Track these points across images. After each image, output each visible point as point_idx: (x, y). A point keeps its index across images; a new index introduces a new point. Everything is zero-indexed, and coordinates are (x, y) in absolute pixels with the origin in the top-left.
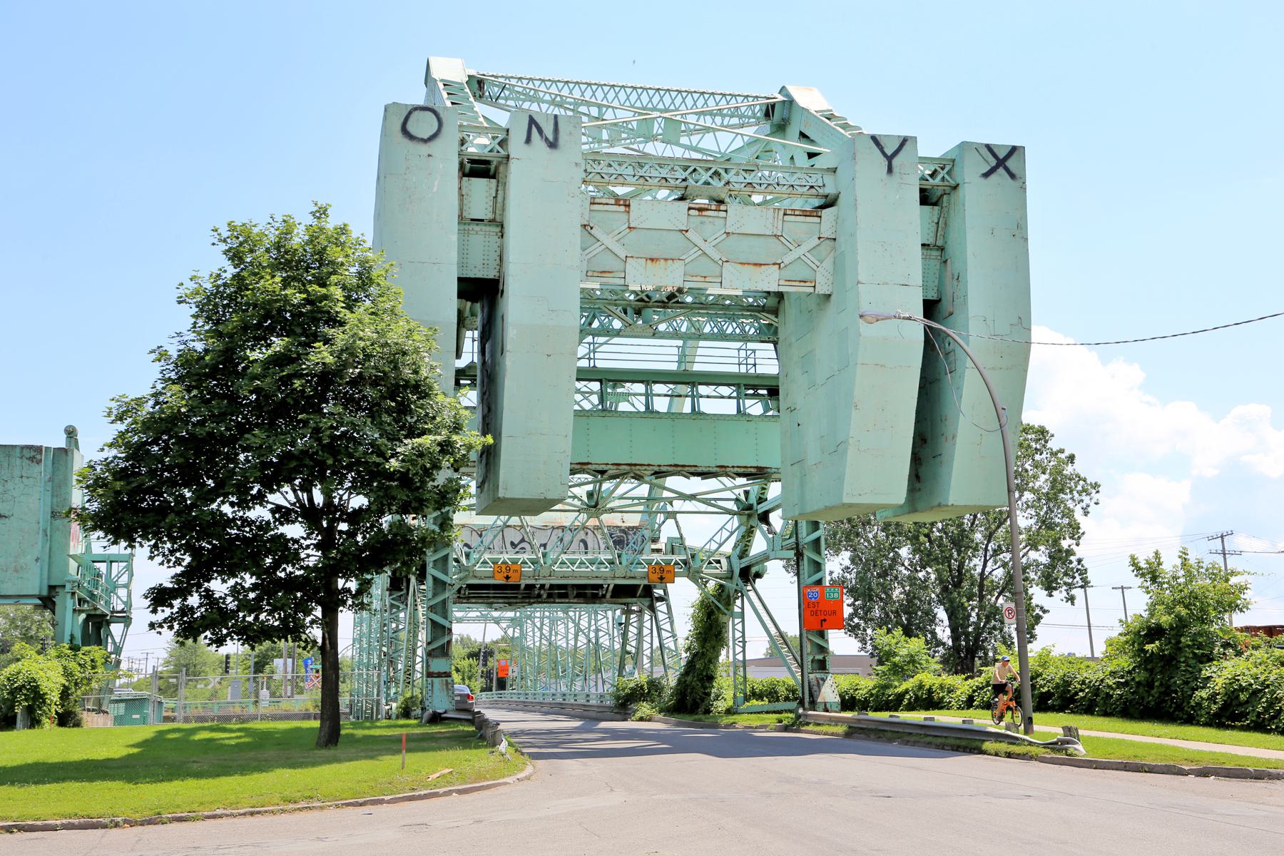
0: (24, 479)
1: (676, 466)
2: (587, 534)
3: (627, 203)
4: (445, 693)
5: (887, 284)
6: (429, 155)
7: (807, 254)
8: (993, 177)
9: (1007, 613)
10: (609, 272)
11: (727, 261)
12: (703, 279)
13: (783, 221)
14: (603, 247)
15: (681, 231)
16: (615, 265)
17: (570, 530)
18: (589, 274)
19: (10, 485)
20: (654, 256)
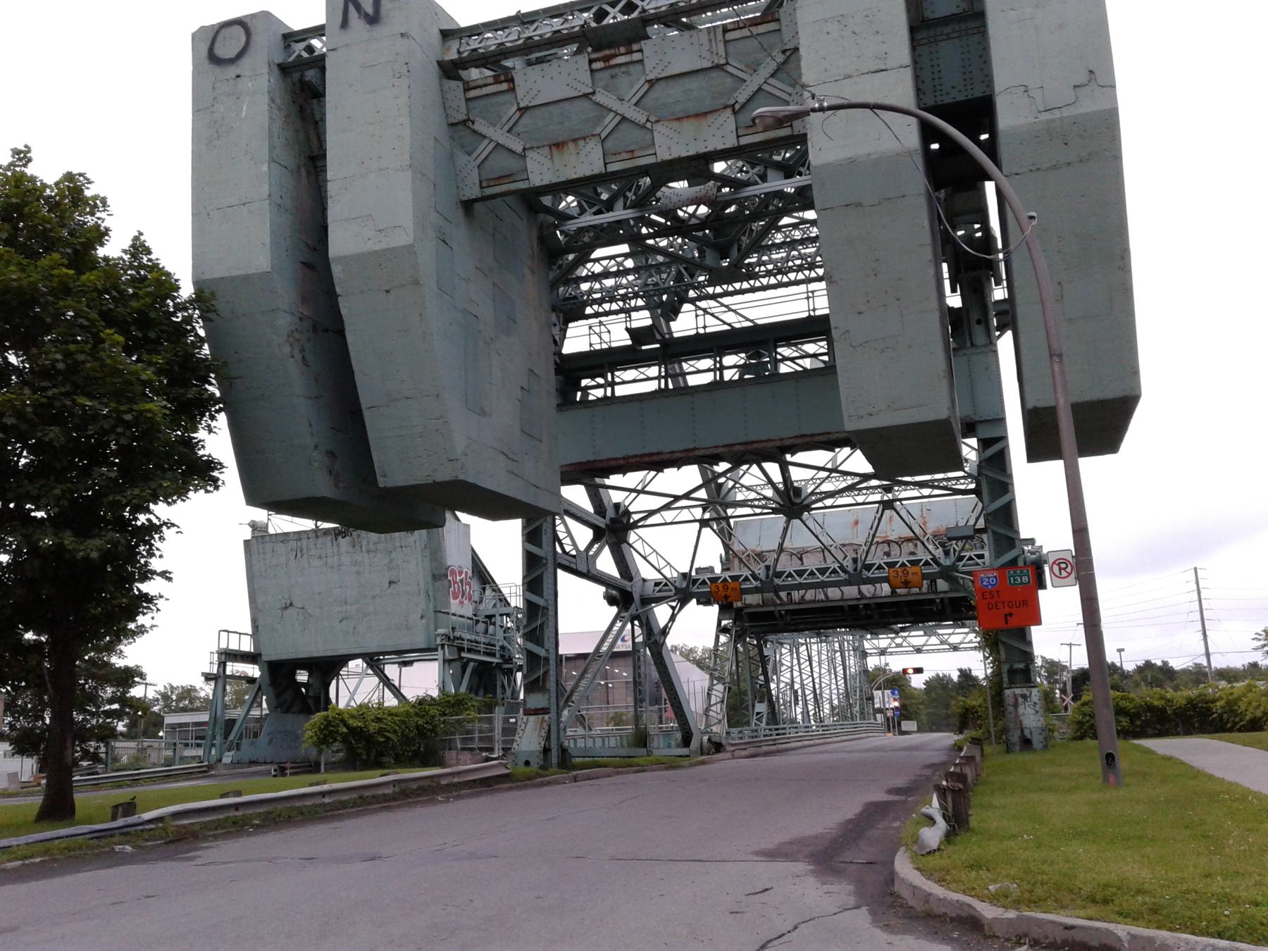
0: (404, 549)
1: (802, 436)
2: (916, 545)
3: (510, 77)
5: (850, 77)
6: (238, 76)
7: (772, 81)
10: (509, 176)
11: (657, 121)
12: (629, 155)
13: (726, 42)
14: (492, 145)
15: (586, 96)
16: (511, 164)
17: (897, 543)
18: (484, 184)
19: (394, 555)
20: (560, 139)
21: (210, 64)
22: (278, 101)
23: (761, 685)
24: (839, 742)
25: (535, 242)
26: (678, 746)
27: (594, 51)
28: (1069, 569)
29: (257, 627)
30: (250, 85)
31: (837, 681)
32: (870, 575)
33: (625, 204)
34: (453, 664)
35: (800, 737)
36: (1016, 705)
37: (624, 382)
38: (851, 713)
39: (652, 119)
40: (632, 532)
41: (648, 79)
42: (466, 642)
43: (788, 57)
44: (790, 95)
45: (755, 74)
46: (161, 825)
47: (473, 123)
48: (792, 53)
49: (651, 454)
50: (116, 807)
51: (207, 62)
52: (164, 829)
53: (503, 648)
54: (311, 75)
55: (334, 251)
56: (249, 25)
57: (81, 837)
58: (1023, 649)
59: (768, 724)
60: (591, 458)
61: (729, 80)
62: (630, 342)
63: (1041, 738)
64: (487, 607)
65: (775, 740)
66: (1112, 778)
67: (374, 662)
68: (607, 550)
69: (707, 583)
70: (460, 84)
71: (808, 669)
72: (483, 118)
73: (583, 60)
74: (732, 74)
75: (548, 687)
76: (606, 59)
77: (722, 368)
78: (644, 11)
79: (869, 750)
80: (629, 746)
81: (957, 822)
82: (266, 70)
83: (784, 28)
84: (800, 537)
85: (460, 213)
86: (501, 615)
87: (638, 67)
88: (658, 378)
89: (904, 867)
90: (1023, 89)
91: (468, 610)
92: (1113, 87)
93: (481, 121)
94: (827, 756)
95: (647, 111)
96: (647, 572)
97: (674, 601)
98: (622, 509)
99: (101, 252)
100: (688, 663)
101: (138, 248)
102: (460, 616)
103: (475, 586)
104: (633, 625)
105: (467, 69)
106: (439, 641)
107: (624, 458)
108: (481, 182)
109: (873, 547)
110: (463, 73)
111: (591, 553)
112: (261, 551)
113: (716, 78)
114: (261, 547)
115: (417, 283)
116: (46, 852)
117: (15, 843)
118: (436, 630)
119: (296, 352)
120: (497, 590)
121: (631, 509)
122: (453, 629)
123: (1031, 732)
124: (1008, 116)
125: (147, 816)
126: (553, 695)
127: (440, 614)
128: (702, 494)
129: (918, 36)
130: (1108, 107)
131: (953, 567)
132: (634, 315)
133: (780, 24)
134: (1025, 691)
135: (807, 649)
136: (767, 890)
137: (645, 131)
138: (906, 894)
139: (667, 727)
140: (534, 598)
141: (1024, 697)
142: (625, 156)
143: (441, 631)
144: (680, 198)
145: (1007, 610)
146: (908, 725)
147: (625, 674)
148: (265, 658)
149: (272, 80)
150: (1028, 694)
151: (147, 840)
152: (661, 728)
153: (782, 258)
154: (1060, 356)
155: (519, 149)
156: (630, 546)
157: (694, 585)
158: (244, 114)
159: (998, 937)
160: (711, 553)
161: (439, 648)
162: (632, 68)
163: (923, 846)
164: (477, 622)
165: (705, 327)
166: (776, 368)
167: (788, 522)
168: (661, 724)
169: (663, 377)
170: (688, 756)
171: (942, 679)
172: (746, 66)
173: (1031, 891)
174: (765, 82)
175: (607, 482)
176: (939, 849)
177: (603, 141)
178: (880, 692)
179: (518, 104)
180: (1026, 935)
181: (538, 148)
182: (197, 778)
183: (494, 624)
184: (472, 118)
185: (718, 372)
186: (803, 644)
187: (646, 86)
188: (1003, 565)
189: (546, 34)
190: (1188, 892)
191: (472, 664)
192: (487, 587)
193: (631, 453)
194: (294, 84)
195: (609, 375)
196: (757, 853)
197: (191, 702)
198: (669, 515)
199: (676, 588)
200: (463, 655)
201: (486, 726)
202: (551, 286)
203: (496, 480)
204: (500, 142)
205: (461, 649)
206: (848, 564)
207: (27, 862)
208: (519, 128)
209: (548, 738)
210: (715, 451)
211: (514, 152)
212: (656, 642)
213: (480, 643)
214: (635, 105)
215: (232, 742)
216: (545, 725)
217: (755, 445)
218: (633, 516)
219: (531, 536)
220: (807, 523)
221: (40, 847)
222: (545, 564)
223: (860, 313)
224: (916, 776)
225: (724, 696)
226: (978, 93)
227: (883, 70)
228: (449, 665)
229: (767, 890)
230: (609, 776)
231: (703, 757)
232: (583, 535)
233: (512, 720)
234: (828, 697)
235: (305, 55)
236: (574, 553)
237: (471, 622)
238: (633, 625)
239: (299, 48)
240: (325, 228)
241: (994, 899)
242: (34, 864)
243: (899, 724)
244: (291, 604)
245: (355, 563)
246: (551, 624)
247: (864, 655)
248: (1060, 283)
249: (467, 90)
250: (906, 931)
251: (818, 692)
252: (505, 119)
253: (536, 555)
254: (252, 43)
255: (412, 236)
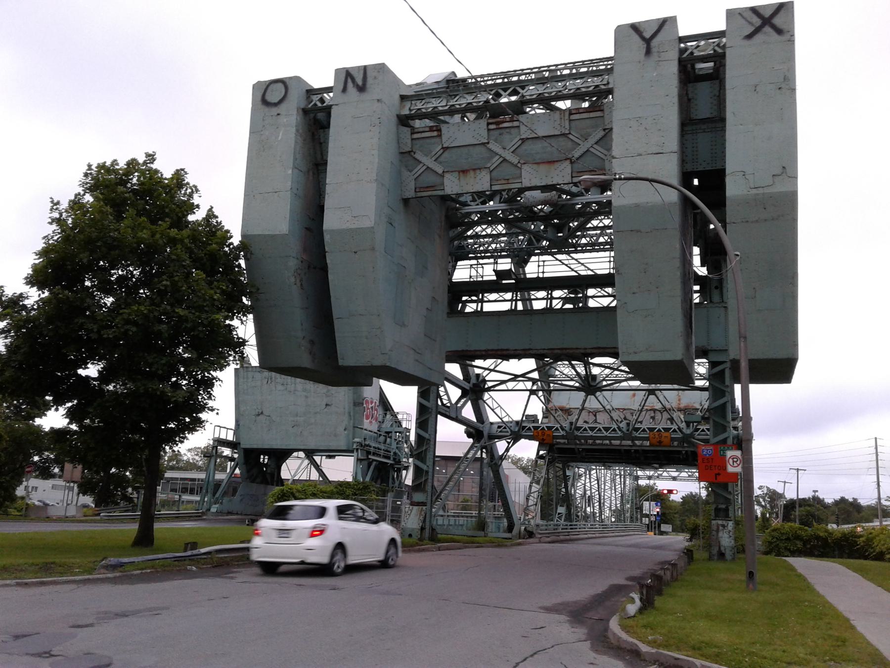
1: (599, 348)
3: (439, 128)
4: (418, 517)
5: (640, 155)
6: (278, 114)
7: (595, 146)
8: (758, 38)
9: (731, 461)
10: (432, 186)
11: (524, 163)
13: (570, 120)
14: (425, 168)
15: (483, 144)
17: (660, 411)
20: (466, 168)
21: (262, 104)
22: (301, 131)
23: (563, 495)
24: (613, 536)
25: (443, 218)
26: (504, 532)
27: (491, 117)
28: (738, 462)
29: (239, 425)
30: (285, 120)
31: (616, 495)
32: (637, 435)
33: (500, 201)
34: (363, 462)
35: (587, 531)
36: (718, 531)
37: (489, 301)
38: (624, 517)
39: (522, 162)
40: (486, 393)
41: (522, 137)
42: (372, 448)
43: (607, 133)
44: (606, 155)
45: (586, 142)
46: (210, 556)
47: (415, 153)
48: (608, 131)
49: (502, 350)
50: (187, 544)
51: (260, 103)
52: (211, 558)
53: (395, 453)
54: (321, 116)
55: (326, 226)
56: (288, 83)
57: (169, 560)
58: (727, 496)
59: (565, 521)
60: (465, 348)
61: (570, 143)
62: (494, 278)
63: (731, 553)
64: (387, 426)
65: (569, 532)
66: (751, 586)
67: (310, 454)
68: (469, 404)
69: (531, 429)
70: (409, 129)
71: (596, 486)
72: (421, 151)
73: (483, 123)
74: (572, 140)
75: (426, 490)
76: (497, 123)
77: (552, 298)
78: (523, 96)
79: (630, 546)
80: (474, 529)
81: (647, 604)
82: (295, 112)
83: (605, 116)
84: (592, 403)
85: (401, 206)
86: (396, 432)
87: (516, 130)
88: (511, 300)
89: (614, 624)
90: (743, 173)
91: (374, 427)
92: (796, 178)
93: (419, 152)
94: (599, 548)
95: (520, 157)
96: (492, 418)
97: (509, 439)
98: (481, 378)
99: (191, 218)
100: (518, 470)
101: (211, 215)
102: (370, 431)
103: (381, 411)
104: (482, 452)
105: (413, 120)
106: (355, 446)
107: (485, 351)
108: (415, 188)
109: (644, 413)
110: (411, 122)
111: (459, 405)
112: (245, 377)
113: (562, 141)
114: (245, 374)
115: (373, 249)
116: (153, 567)
117: (136, 560)
118: (354, 439)
119: (298, 281)
120: (394, 415)
121: (487, 378)
122: (365, 439)
123: (725, 550)
124: (733, 188)
125: (203, 550)
126: (430, 494)
127: (356, 429)
128: (535, 375)
129: (686, 129)
130: (792, 190)
131: (692, 435)
132: (500, 261)
133: (604, 113)
134: (724, 523)
135: (597, 472)
136: (542, 627)
137: (517, 168)
138: (611, 636)
139: (498, 514)
140: (422, 433)
141: (723, 526)
142: (504, 182)
143: (357, 440)
144: (535, 200)
145: (717, 471)
146: (665, 527)
147: (472, 472)
148: (243, 446)
149: (298, 119)
150: (726, 525)
151: (203, 564)
152: (494, 514)
153: (596, 234)
154: (745, 338)
155: (440, 171)
156: (484, 402)
157: (523, 430)
158: (280, 138)
159: (647, 661)
160: (536, 407)
161: (355, 451)
162: (513, 130)
163: (626, 614)
164: (380, 435)
165: (543, 272)
166: (586, 303)
167: (586, 397)
168: (491, 511)
169: (514, 300)
170: (511, 539)
171: (694, 496)
172: (581, 136)
173: (667, 641)
174: (591, 147)
175: (474, 363)
176: (634, 616)
177: (491, 172)
178: (648, 503)
179: (442, 145)
180: (658, 661)
181: (452, 172)
182: (195, 520)
183: (391, 437)
184: (414, 151)
185: (549, 301)
186: (594, 469)
187: (520, 142)
188: (717, 442)
189: (463, 104)
190: (737, 649)
191: (374, 463)
192: (388, 413)
193: (490, 348)
194: (310, 120)
195: (481, 295)
196: (541, 608)
197: (177, 463)
198: (511, 385)
199: (511, 431)
200: (370, 457)
201: (381, 504)
202: (451, 241)
203: (408, 366)
204: (429, 166)
205: (368, 453)
206: (623, 425)
207: (144, 571)
208: (441, 159)
209: (424, 521)
210: (542, 352)
211: (437, 173)
212: (496, 464)
213: (381, 450)
214: (512, 152)
215: (217, 498)
216: (423, 513)
217: (568, 351)
218: (488, 383)
219: (423, 395)
220: (599, 398)
221: (150, 563)
222: (431, 413)
223: (634, 293)
224: (649, 569)
225: (537, 501)
226: (719, 167)
227: (660, 153)
228: (361, 462)
229: (542, 627)
230: (460, 549)
231: (520, 540)
232: (455, 393)
233: (398, 503)
234: (609, 506)
235: (319, 104)
236: (449, 405)
237: (376, 435)
238: (482, 452)
239: (315, 98)
240: (321, 209)
241: (649, 643)
242: (147, 573)
243: (659, 526)
244: (262, 413)
245: (305, 390)
246: (432, 450)
247: (637, 478)
248: (754, 288)
249: (412, 133)
250: (605, 654)
251: (602, 501)
252: (434, 153)
253: (426, 406)
254: (289, 95)
255: (373, 222)
